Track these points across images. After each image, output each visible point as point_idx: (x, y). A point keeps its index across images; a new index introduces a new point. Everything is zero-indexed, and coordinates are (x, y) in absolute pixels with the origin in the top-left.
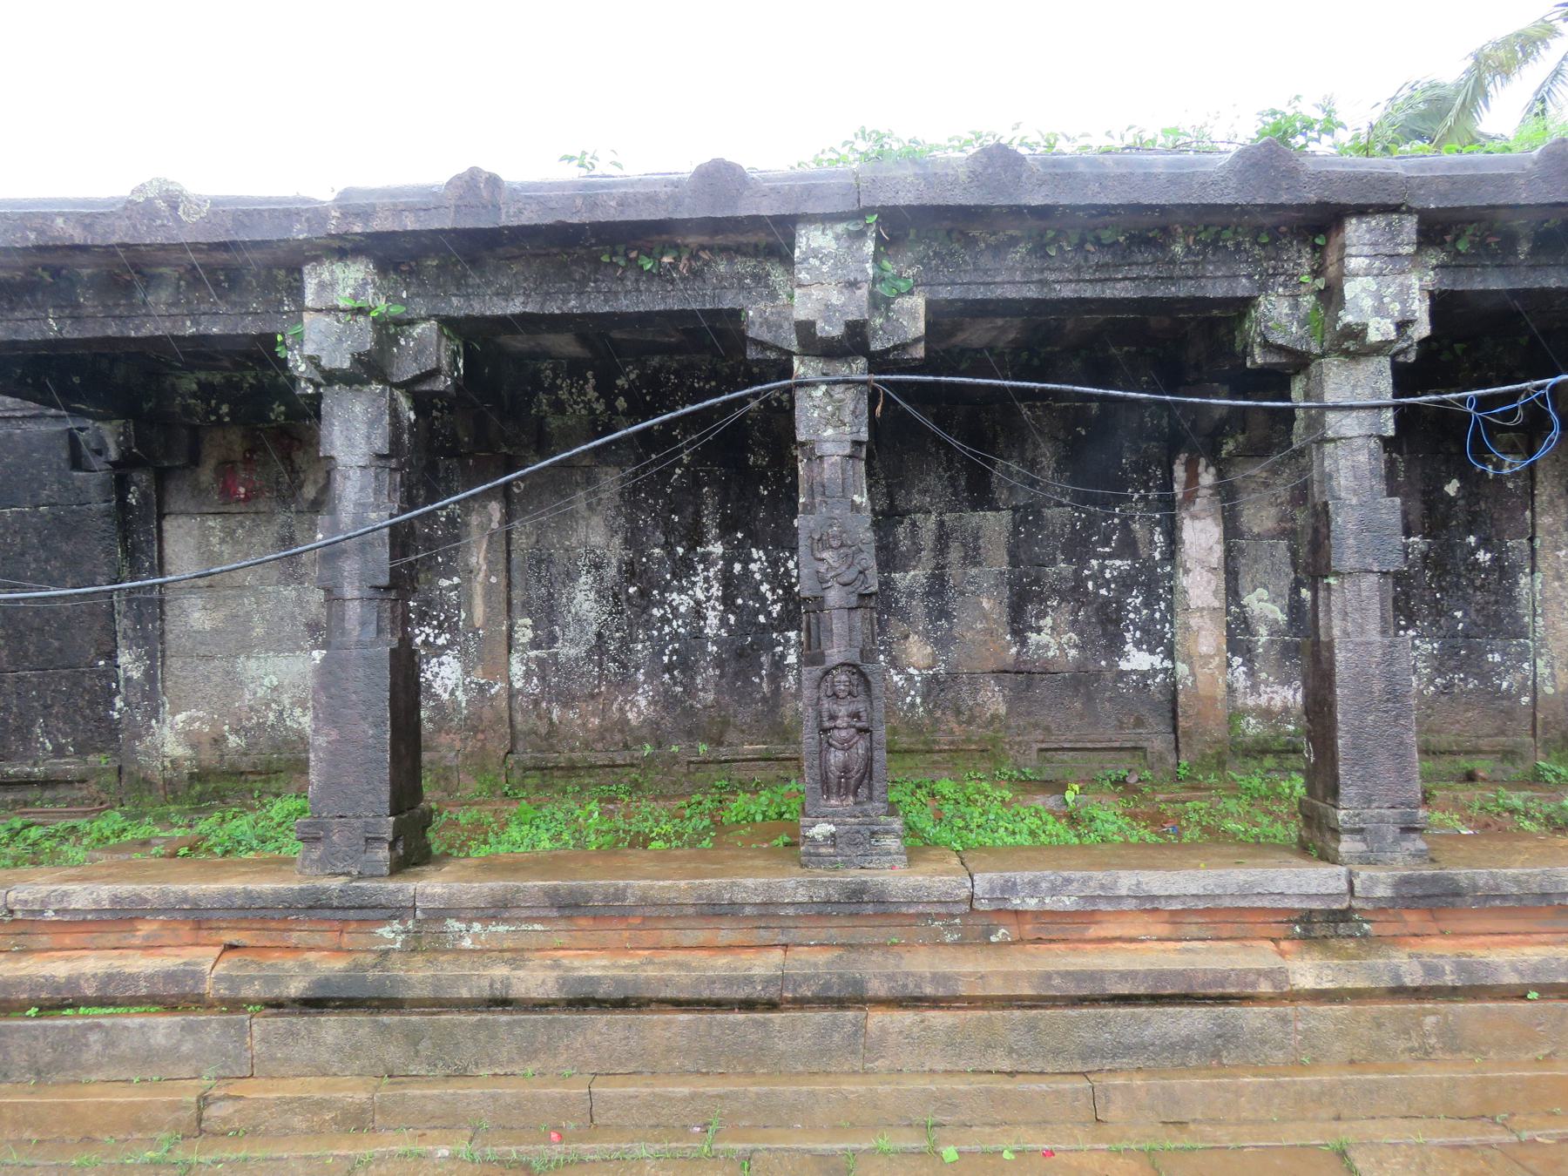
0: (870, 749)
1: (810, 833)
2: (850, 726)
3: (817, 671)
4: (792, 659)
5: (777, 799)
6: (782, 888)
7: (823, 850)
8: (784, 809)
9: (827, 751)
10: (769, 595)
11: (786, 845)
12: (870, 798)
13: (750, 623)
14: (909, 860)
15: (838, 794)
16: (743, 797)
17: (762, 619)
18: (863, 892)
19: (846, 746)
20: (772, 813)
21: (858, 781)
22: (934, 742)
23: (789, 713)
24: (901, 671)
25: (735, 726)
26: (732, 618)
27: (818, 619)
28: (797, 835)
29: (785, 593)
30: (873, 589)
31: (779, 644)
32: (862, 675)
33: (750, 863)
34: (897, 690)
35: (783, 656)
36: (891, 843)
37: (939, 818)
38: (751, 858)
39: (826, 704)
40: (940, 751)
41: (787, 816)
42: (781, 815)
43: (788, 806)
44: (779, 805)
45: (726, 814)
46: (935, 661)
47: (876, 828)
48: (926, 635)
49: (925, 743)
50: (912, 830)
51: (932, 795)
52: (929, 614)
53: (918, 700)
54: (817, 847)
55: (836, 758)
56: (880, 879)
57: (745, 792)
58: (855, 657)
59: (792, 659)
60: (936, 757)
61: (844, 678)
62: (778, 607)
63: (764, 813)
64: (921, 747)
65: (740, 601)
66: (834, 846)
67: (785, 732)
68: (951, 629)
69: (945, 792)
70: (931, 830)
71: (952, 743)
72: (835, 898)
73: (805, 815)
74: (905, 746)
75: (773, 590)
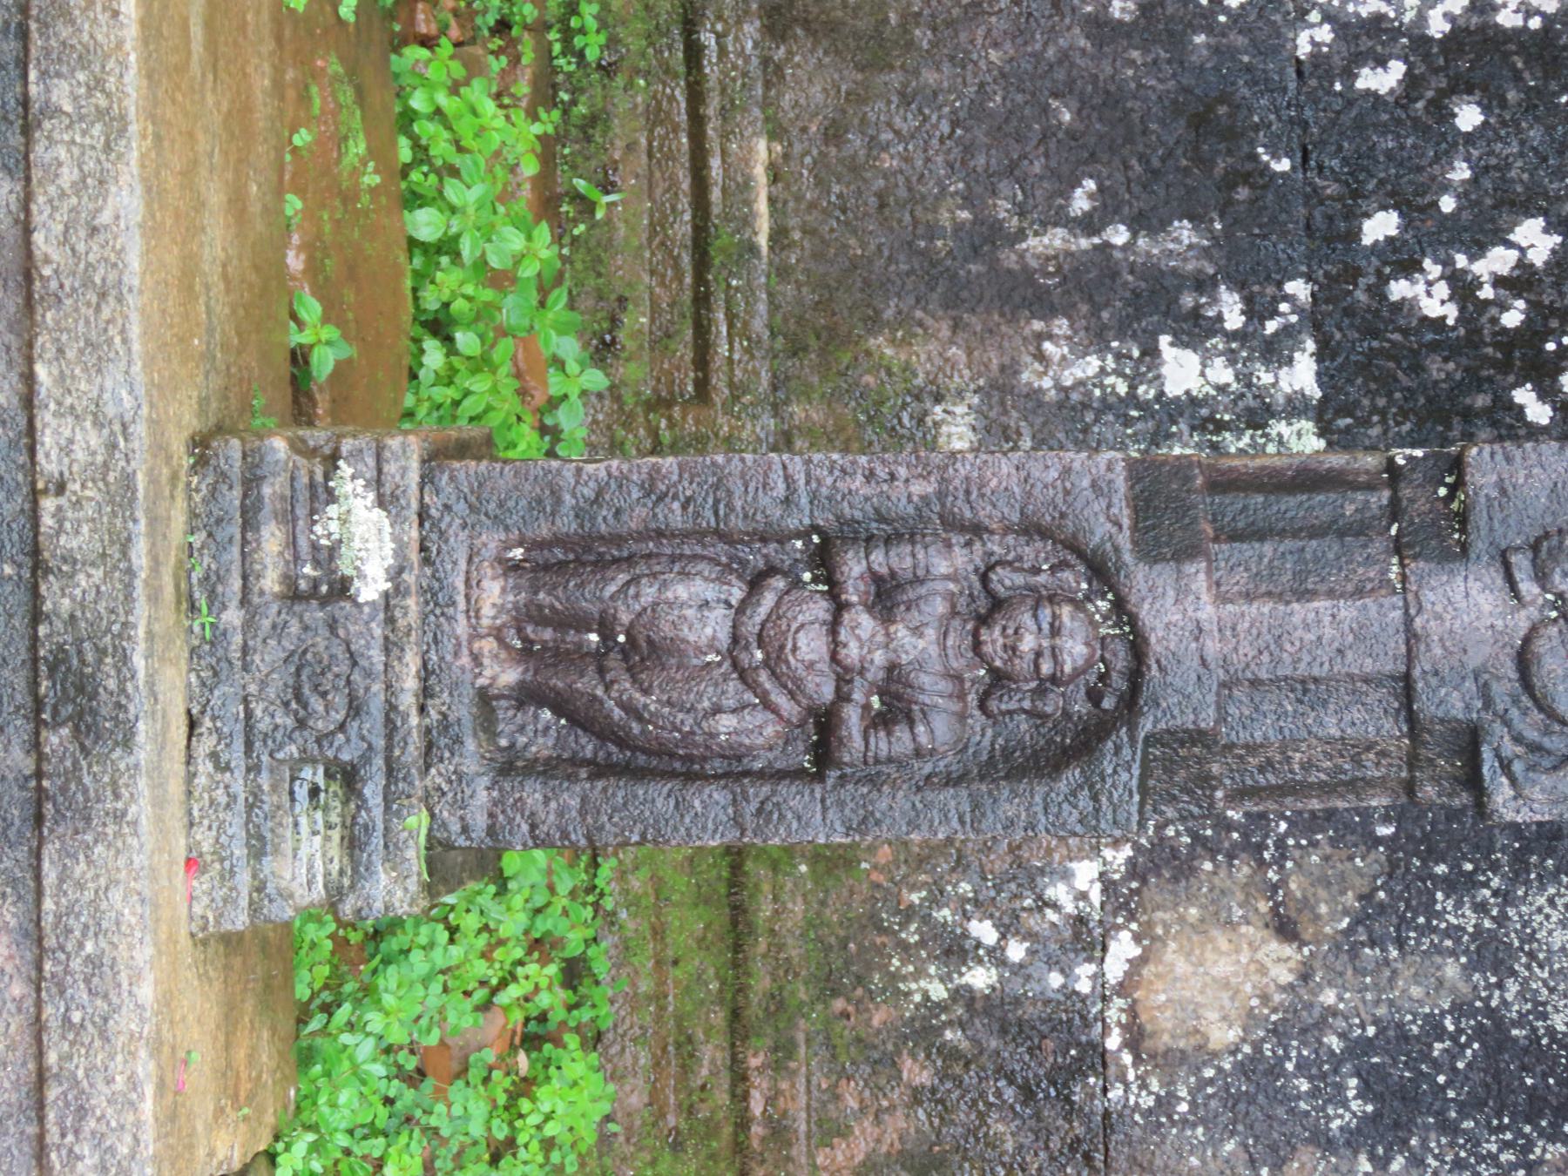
0: (735, 769)
1: (351, 485)
2: (844, 676)
3: (1108, 523)
4: (1182, 371)
5: (513, 308)
6: (97, 352)
7: (271, 539)
8: (466, 340)
9: (727, 569)
10: (1499, 260)
11: (299, 358)
12: (509, 767)
13: (1359, 164)
14: (231, 941)
15: (529, 615)
16: (523, 137)
17: (1381, 226)
18: (86, 727)
19: (754, 658)
20: (449, 285)
21: (587, 713)
22: (783, 1050)
23: (923, 357)
24: (1122, 898)
25: (858, 97)
26: (1383, 79)
27: (1360, 529)
28: (342, 411)
29: (1508, 340)
30: (1501, 795)
31: (1256, 311)
32: (1078, 745)
33: (216, 197)
34: (1027, 877)
35: (1197, 331)
36: (306, 859)
37: (426, 1068)
38: (237, 203)
39: (949, 564)
40: (740, 1077)
41: (434, 356)
42: (439, 326)
43: (481, 364)
44: (483, 314)
45: (441, 64)
46: (1169, 1062)
47: (373, 791)
48: (1296, 1022)
49: (777, 1004)
50: (367, 945)
51: (535, 1035)
52: (1395, 1038)
53: (980, 978)
54: (288, 517)
55: (698, 608)
56: (141, 810)
57: (547, 148)
58: (1180, 701)
59: (1182, 371)
60: (711, 1054)
61: (1075, 650)
62: (1436, 303)
63: (448, 247)
64: (761, 983)
65: (1468, 117)
66: (293, 595)
67: (833, 338)
68: (1326, 1143)
69: (547, 1097)
70: (360, 1049)
71: (779, 1131)
72: (57, 599)
73: (437, 457)
74: (765, 910)
75: (1520, 282)
